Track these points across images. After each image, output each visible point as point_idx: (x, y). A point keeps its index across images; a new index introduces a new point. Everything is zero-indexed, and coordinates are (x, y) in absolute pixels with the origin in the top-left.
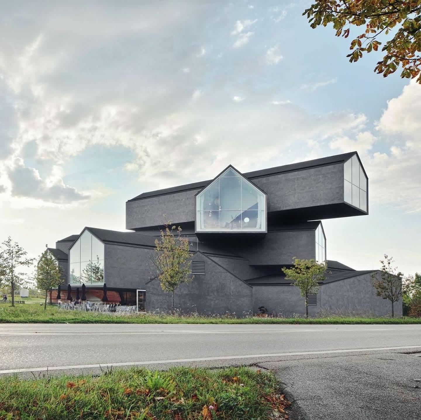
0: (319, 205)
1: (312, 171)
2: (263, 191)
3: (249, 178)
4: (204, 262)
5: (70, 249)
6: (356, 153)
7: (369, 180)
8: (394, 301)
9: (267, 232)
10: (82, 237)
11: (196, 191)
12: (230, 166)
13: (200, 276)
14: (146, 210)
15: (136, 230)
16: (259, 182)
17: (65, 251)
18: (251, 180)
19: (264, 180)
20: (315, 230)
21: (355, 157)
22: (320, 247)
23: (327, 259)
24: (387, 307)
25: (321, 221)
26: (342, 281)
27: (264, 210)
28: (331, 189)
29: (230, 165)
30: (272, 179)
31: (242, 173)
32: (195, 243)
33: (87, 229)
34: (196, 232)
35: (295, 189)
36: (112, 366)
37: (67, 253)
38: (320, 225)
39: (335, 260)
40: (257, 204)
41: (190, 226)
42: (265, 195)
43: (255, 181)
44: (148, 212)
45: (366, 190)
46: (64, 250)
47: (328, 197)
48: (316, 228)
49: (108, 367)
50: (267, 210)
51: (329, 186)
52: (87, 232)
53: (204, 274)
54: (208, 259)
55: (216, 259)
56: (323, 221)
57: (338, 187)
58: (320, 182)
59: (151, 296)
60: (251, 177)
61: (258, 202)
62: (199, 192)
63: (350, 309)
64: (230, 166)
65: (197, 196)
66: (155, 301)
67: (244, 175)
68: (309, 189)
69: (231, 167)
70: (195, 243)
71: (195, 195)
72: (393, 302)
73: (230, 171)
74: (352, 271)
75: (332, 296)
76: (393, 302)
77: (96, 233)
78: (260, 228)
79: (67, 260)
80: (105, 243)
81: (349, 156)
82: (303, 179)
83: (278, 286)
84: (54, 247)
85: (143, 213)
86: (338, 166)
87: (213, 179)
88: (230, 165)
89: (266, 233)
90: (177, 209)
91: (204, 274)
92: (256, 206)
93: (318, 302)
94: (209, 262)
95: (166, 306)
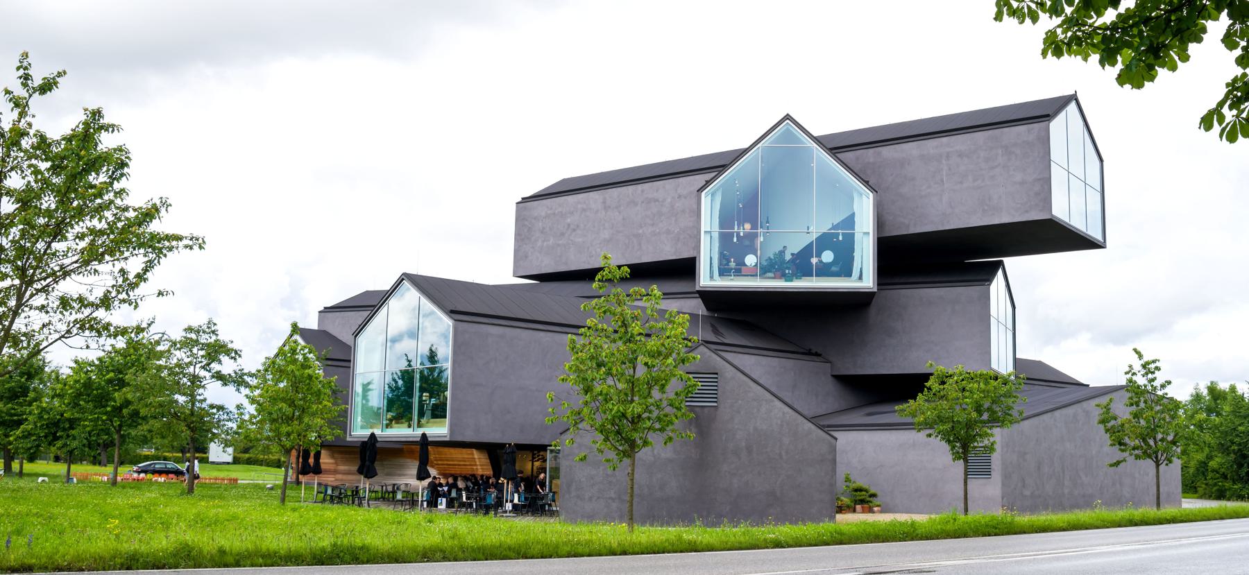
0: (996, 221)
1: (980, 136)
2: (866, 183)
3: (831, 149)
4: (717, 374)
5: (357, 334)
6: (1074, 98)
7: (1104, 163)
8: (1161, 462)
9: (875, 290)
10: (393, 302)
11: (700, 179)
12: (788, 117)
13: (706, 410)
14: (569, 225)
15: (543, 278)
16: (857, 159)
17: (346, 337)
18: (838, 155)
19: (869, 154)
20: (990, 285)
21: (1073, 105)
22: (1002, 328)
23: (1017, 357)
24: (1148, 475)
25: (1002, 261)
26: (1049, 414)
27: (869, 233)
28: (1022, 183)
29: (788, 115)
30: (888, 152)
31: (815, 135)
32: (694, 317)
33: (406, 277)
34: (697, 288)
35: (942, 181)
36: (283, 500)
37: (350, 343)
38: (1000, 272)
39: (1037, 359)
40: (853, 215)
41: (685, 269)
42: (871, 195)
43: (848, 156)
44: (574, 230)
45: (1099, 188)
46: (340, 328)
47: (1018, 203)
48: (990, 280)
49: (283, 500)
50: (876, 232)
51: (1018, 177)
52: (406, 283)
53: (715, 404)
54: (718, 359)
55: (748, 361)
56: (1008, 261)
57: (1039, 179)
58: (999, 164)
59: (575, 467)
60: (839, 146)
61: (855, 211)
62: (708, 183)
63: (1066, 483)
64: (788, 117)
65: (703, 193)
66: (583, 479)
67: (818, 140)
68: (975, 181)
69: (788, 119)
70: (694, 317)
71: (698, 191)
72: (1158, 465)
73: (788, 129)
74: (1082, 387)
75: (1025, 453)
76: (1158, 465)
77: (431, 288)
78: (860, 278)
79: (350, 361)
80: (455, 320)
81: (1060, 104)
82: (959, 156)
83: (843, 432)
84: (312, 323)
85: (563, 234)
86: (1036, 127)
87: (746, 146)
88: (788, 115)
89: (875, 292)
90: (653, 225)
91: (715, 404)
92: (850, 221)
93: (994, 469)
94: (729, 372)
95: (612, 492)
